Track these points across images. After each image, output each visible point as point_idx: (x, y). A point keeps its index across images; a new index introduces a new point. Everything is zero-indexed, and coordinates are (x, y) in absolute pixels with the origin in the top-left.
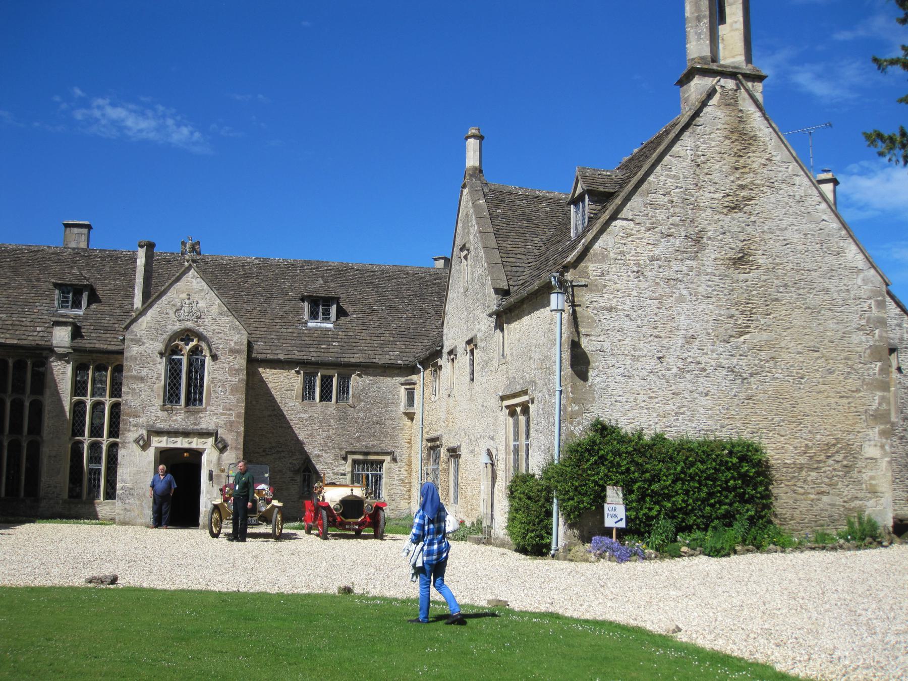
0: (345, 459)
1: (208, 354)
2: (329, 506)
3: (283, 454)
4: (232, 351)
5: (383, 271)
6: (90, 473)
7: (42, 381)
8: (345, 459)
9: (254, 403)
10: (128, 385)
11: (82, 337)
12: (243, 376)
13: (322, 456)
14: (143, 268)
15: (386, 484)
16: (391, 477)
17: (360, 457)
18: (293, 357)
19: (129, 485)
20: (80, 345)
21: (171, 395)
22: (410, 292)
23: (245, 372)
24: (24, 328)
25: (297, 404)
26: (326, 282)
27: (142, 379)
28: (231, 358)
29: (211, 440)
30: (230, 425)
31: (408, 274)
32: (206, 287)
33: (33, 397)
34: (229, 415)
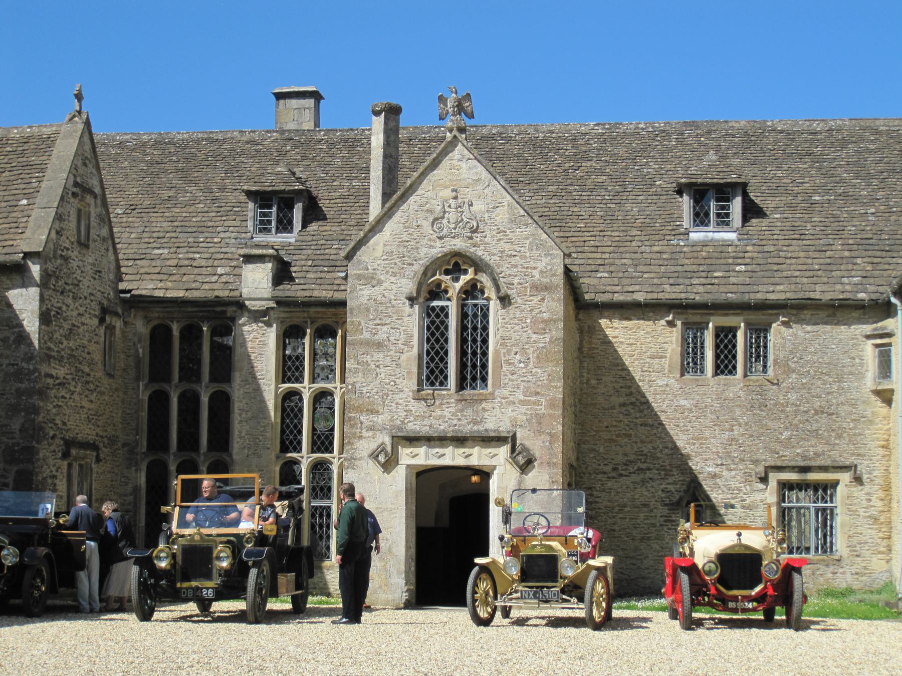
0: (764, 480)
1: (493, 296)
2: (694, 566)
3: (648, 475)
4: (537, 288)
5: (830, 130)
6: (313, 516)
7: (226, 361)
8: (764, 480)
9: (593, 382)
10: (356, 357)
11: (292, 279)
13: (720, 476)
15: (842, 525)
16: (852, 513)
17: (793, 476)
18: (661, 296)
20: (288, 294)
21: (432, 372)
22: (882, 166)
23: (561, 325)
24: (196, 271)
25: (673, 381)
26: (723, 157)
27: (379, 345)
28: (536, 299)
29: (504, 451)
31: (877, 132)
32: (485, 175)
33: (215, 387)
34: (535, 403)
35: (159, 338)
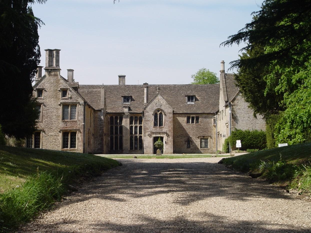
12: (172, 119)
14: (146, 93)
17: (202, 138)
19: (147, 145)
30: (170, 131)
35: (112, 118)
